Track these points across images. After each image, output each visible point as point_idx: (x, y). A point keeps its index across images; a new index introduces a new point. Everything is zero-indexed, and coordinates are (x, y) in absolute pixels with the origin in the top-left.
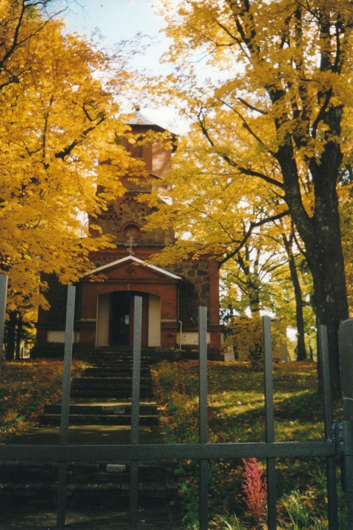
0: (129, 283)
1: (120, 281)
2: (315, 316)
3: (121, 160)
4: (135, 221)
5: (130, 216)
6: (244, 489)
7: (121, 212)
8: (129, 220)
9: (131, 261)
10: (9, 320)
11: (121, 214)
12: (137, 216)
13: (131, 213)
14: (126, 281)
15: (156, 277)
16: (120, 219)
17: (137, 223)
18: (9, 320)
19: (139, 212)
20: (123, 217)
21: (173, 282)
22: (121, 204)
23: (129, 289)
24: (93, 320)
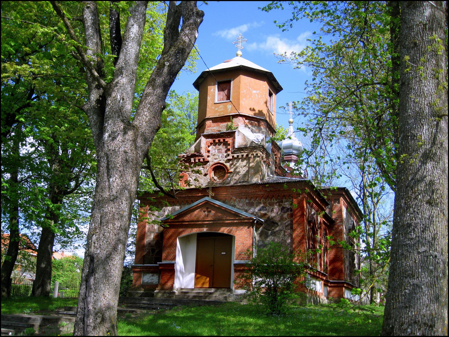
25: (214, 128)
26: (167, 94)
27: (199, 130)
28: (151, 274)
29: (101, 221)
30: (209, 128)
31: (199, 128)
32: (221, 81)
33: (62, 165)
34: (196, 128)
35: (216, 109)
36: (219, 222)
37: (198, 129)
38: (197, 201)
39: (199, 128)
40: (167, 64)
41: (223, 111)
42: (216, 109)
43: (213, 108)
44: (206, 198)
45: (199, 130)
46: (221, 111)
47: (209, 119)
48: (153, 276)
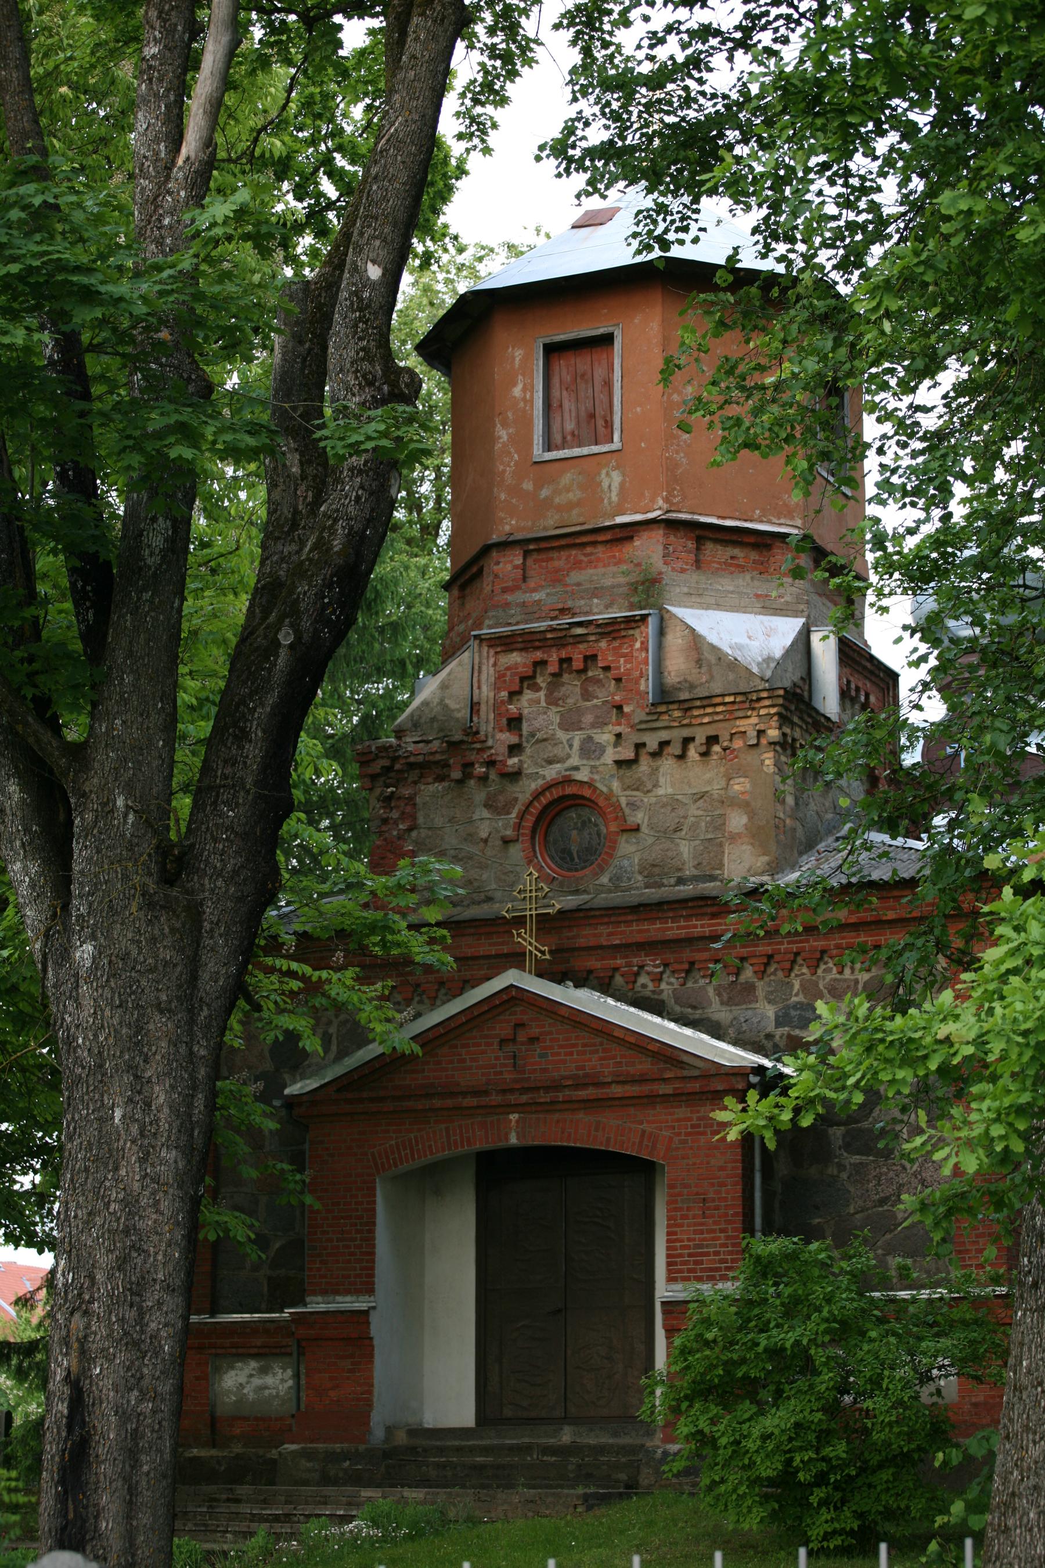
0: (515, 1107)
1: (473, 1101)
2: (188, 801)
3: (48, 1358)
4: (582, 776)
5: (558, 751)
6: (664, 1472)
7: (514, 739)
8: (551, 773)
9: (513, 996)
10: (644, 183)
11: (515, 749)
12: (590, 750)
13: (562, 735)
14: (495, 1099)
15: (643, 1065)
16: (515, 776)
17: (590, 784)
18: (644, 183)
19: (600, 724)
20: (525, 761)
21: (632, 1040)
22: (515, 694)
23: (513, 1140)
24: (360, 1304)
25: (536, 596)
26: (344, 1485)
27: (462, 597)
28: (253, 1364)
29: (475, 958)
30: (509, 598)
31: (463, 588)
32: (562, 337)
33: (1002, 1313)
34: (447, 586)
35: (544, 493)
36: (583, 1094)
37: (456, 592)
38: (488, 978)
39: (463, 588)
40: (286, 638)
41: (579, 503)
42: (544, 493)
43: (528, 486)
44: (511, 977)
45: (462, 597)
46: (570, 506)
47: (505, 545)
48: (264, 1371)
